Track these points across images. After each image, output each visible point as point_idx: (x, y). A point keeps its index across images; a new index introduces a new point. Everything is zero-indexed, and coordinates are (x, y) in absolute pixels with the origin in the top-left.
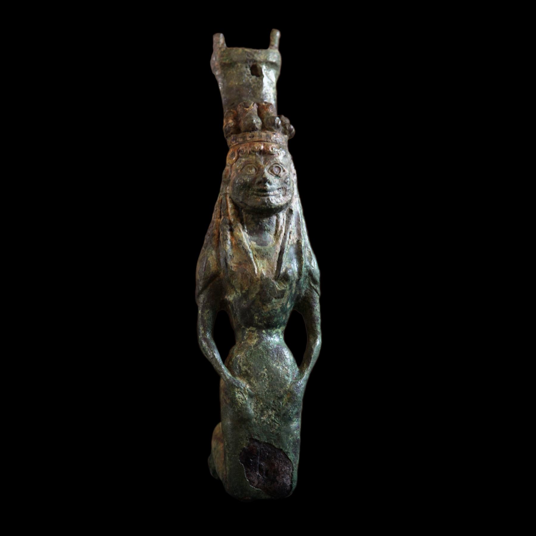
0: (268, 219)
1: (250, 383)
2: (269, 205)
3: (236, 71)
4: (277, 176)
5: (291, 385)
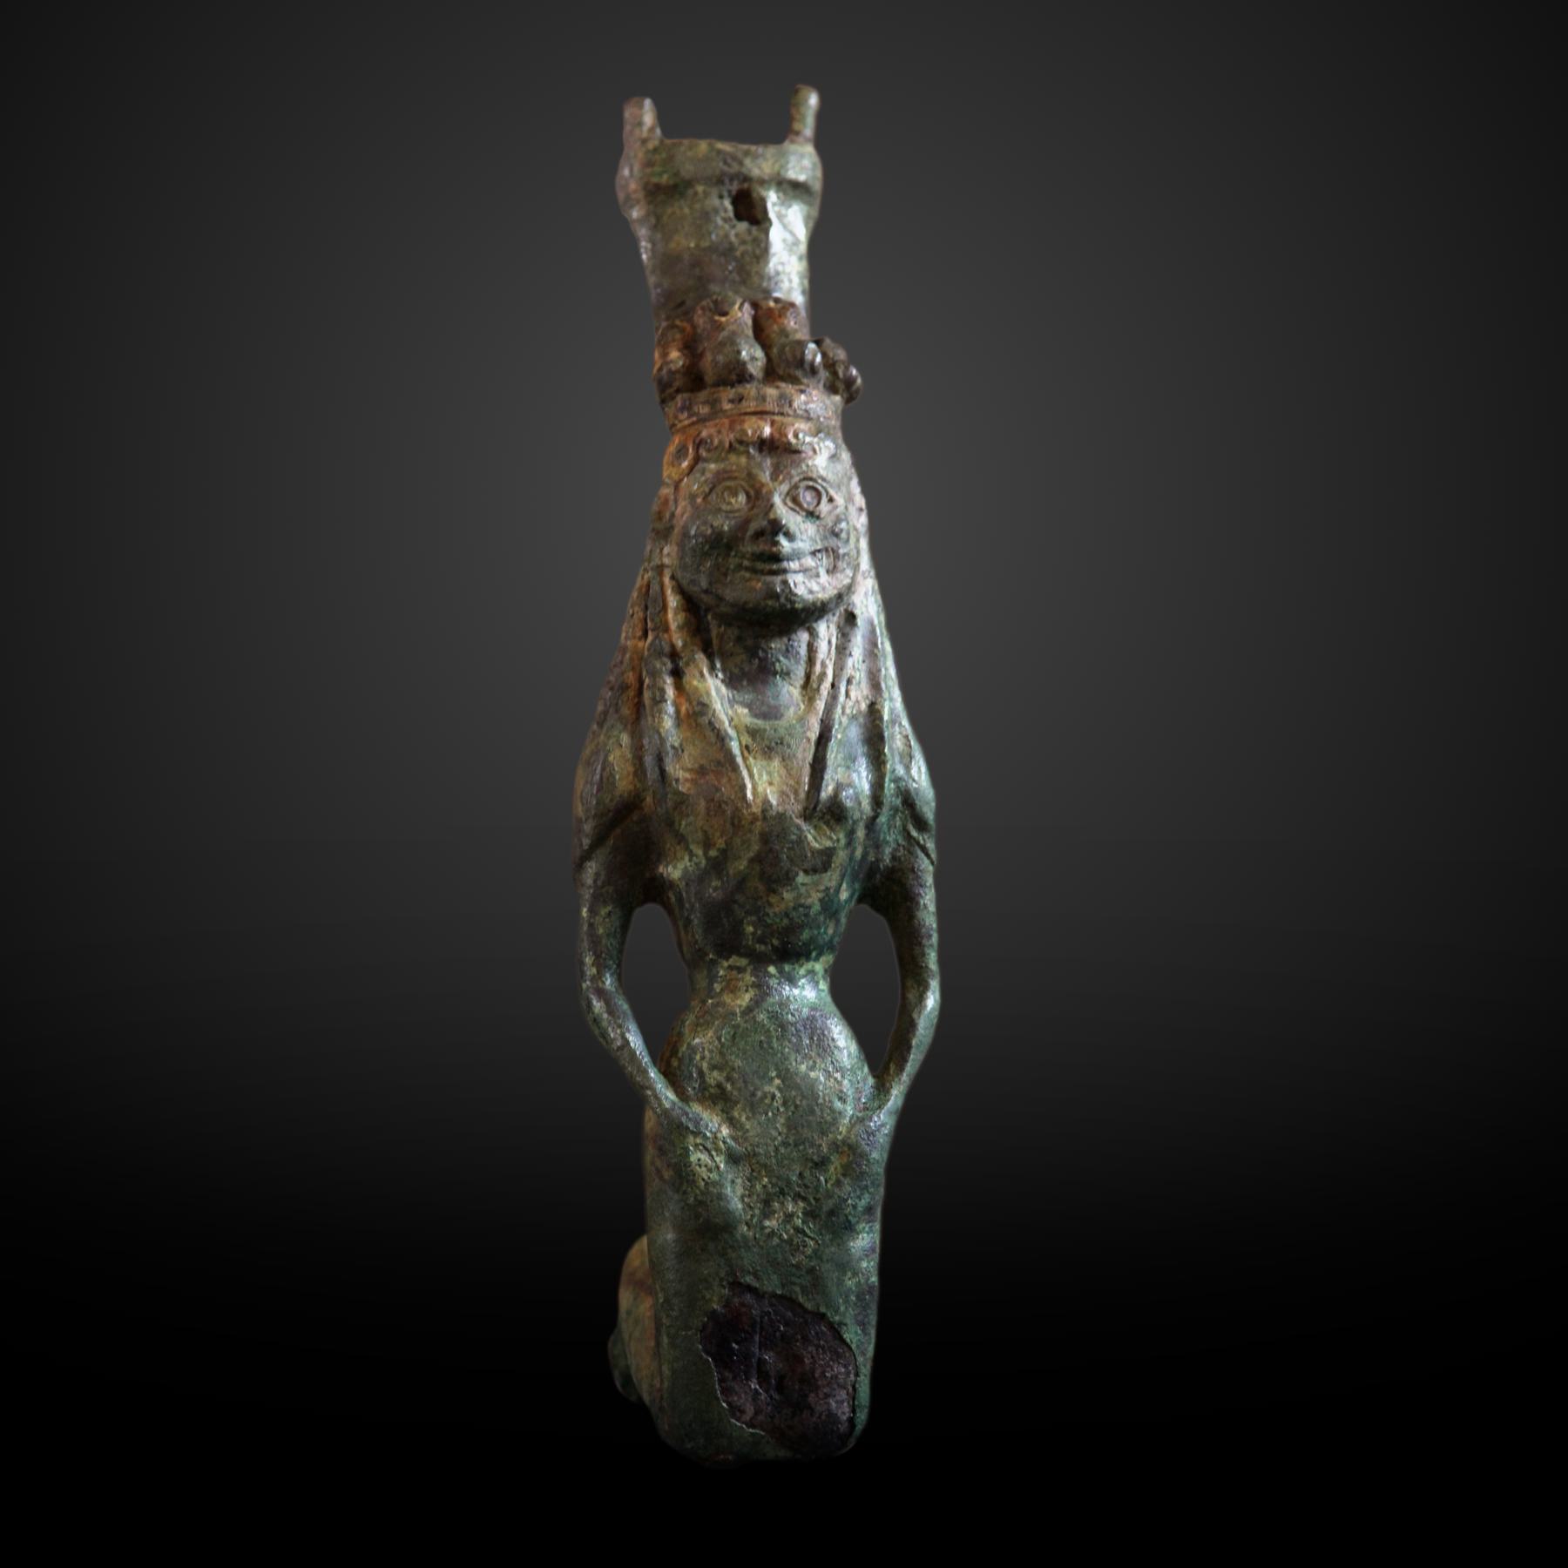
0: (785, 640)
1: (732, 1122)
2: (787, 599)
3: (691, 208)
4: (812, 515)
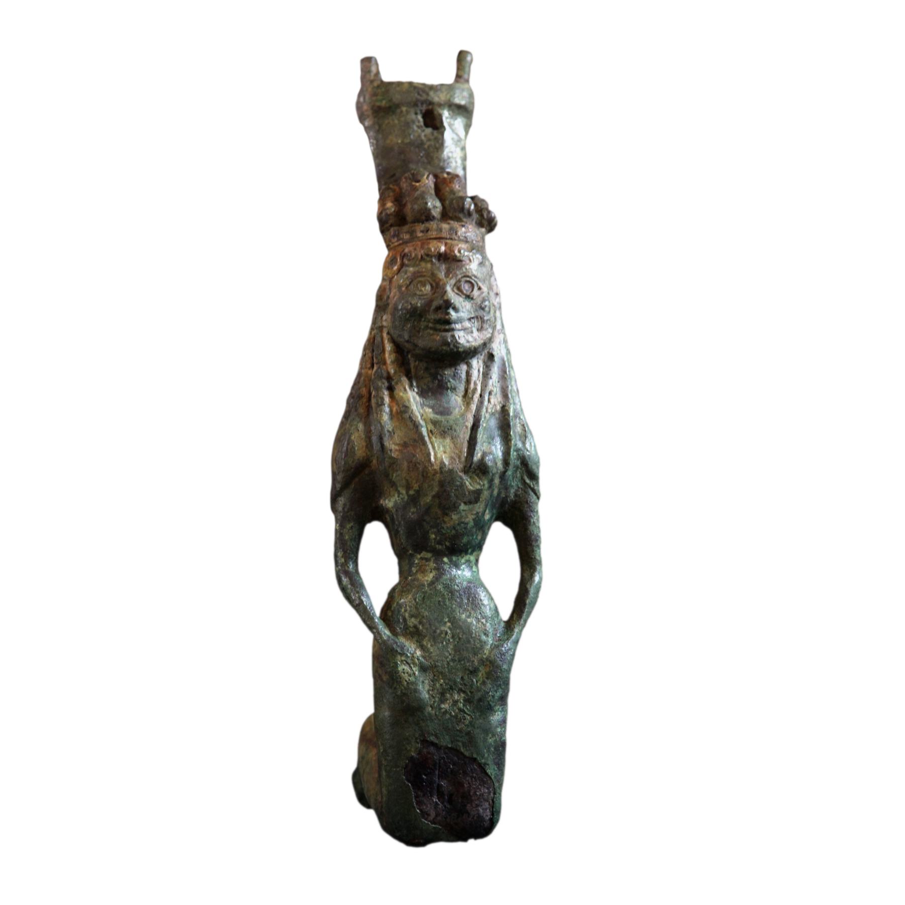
0: (453, 369)
1: (422, 648)
2: (454, 346)
3: (399, 120)
4: (468, 297)
5: (492, 650)
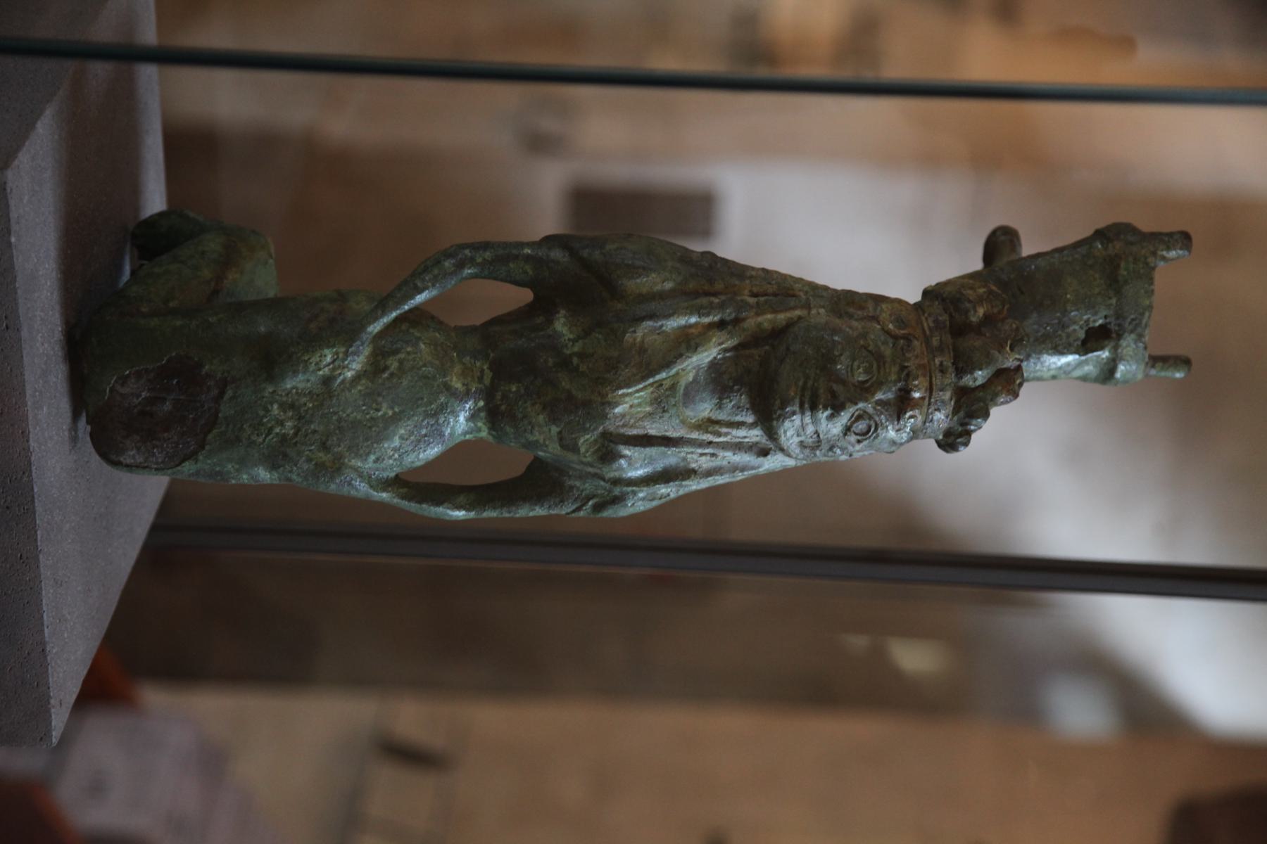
1: (357, 378)
2: (780, 416)
3: (1099, 294)
4: (847, 430)
5: (356, 469)
